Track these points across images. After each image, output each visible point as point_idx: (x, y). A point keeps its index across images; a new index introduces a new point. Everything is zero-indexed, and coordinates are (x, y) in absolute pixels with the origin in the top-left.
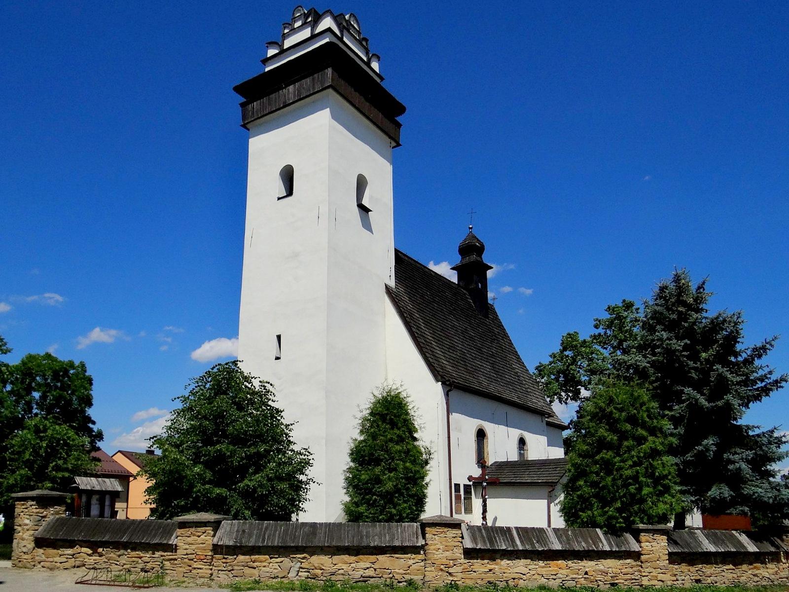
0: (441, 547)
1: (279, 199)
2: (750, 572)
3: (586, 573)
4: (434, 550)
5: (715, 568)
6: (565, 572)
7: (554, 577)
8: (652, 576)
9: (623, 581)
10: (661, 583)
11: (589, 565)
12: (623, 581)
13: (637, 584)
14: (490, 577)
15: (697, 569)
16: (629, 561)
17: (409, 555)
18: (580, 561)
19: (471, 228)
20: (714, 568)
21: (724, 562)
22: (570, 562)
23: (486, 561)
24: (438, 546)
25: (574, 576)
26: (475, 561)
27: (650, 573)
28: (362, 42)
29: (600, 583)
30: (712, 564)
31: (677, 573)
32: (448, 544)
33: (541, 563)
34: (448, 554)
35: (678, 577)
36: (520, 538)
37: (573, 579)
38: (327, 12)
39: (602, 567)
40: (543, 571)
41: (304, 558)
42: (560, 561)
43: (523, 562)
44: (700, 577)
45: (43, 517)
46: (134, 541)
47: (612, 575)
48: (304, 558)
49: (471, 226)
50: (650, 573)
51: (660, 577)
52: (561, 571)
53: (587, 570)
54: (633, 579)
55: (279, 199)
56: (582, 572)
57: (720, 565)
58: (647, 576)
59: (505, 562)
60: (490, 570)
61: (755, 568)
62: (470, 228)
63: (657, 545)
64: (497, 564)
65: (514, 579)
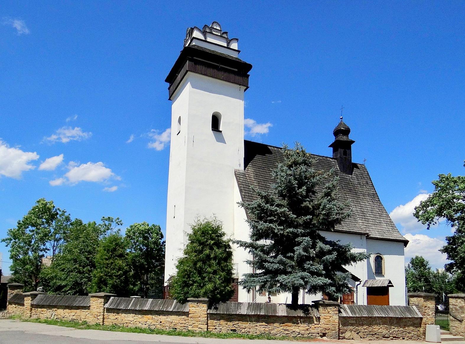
0: (95, 307)
1: (177, 134)
2: (282, 328)
3: (161, 322)
4: (93, 308)
5: (250, 324)
6: (151, 321)
7: (145, 323)
8: (194, 325)
9: (179, 327)
10: (200, 330)
11: (162, 318)
12: (179, 327)
13: (187, 329)
14: (115, 322)
15: (233, 324)
16: (183, 317)
17: (86, 310)
18: (158, 316)
19: (342, 118)
20: (249, 324)
21: (258, 321)
22: (154, 316)
23: (115, 314)
24: (94, 307)
25: (155, 323)
26: (110, 314)
27: (194, 323)
28: (223, 35)
29: (167, 327)
30: (248, 321)
31: (216, 325)
32: (98, 306)
33: (140, 316)
34: (98, 310)
35: (216, 327)
36: (133, 303)
37: (154, 325)
38: (213, 23)
39: (169, 320)
40: (140, 320)
41: (56, 310)
42: (149, 316)
43: (132, 315)
44: (235, 328)
45: (12, 293)
46: (75, 305)
47: (175, 324)
48: (56, 310)
49: (341, 117)
50: (194, 323)
51: (200, 326)
52: (149, 320)
53: (161, 320)
54: (185, 327)
55: (177, 134)
56: (159, 322)
57: (255, 323)
58: (191, 325)
59: (123, 315)
60: (117, 318)
61: (287, 325)
62: (341, 119)
63: (199, 309)
64: (120, 316)
65: (127, 323)
